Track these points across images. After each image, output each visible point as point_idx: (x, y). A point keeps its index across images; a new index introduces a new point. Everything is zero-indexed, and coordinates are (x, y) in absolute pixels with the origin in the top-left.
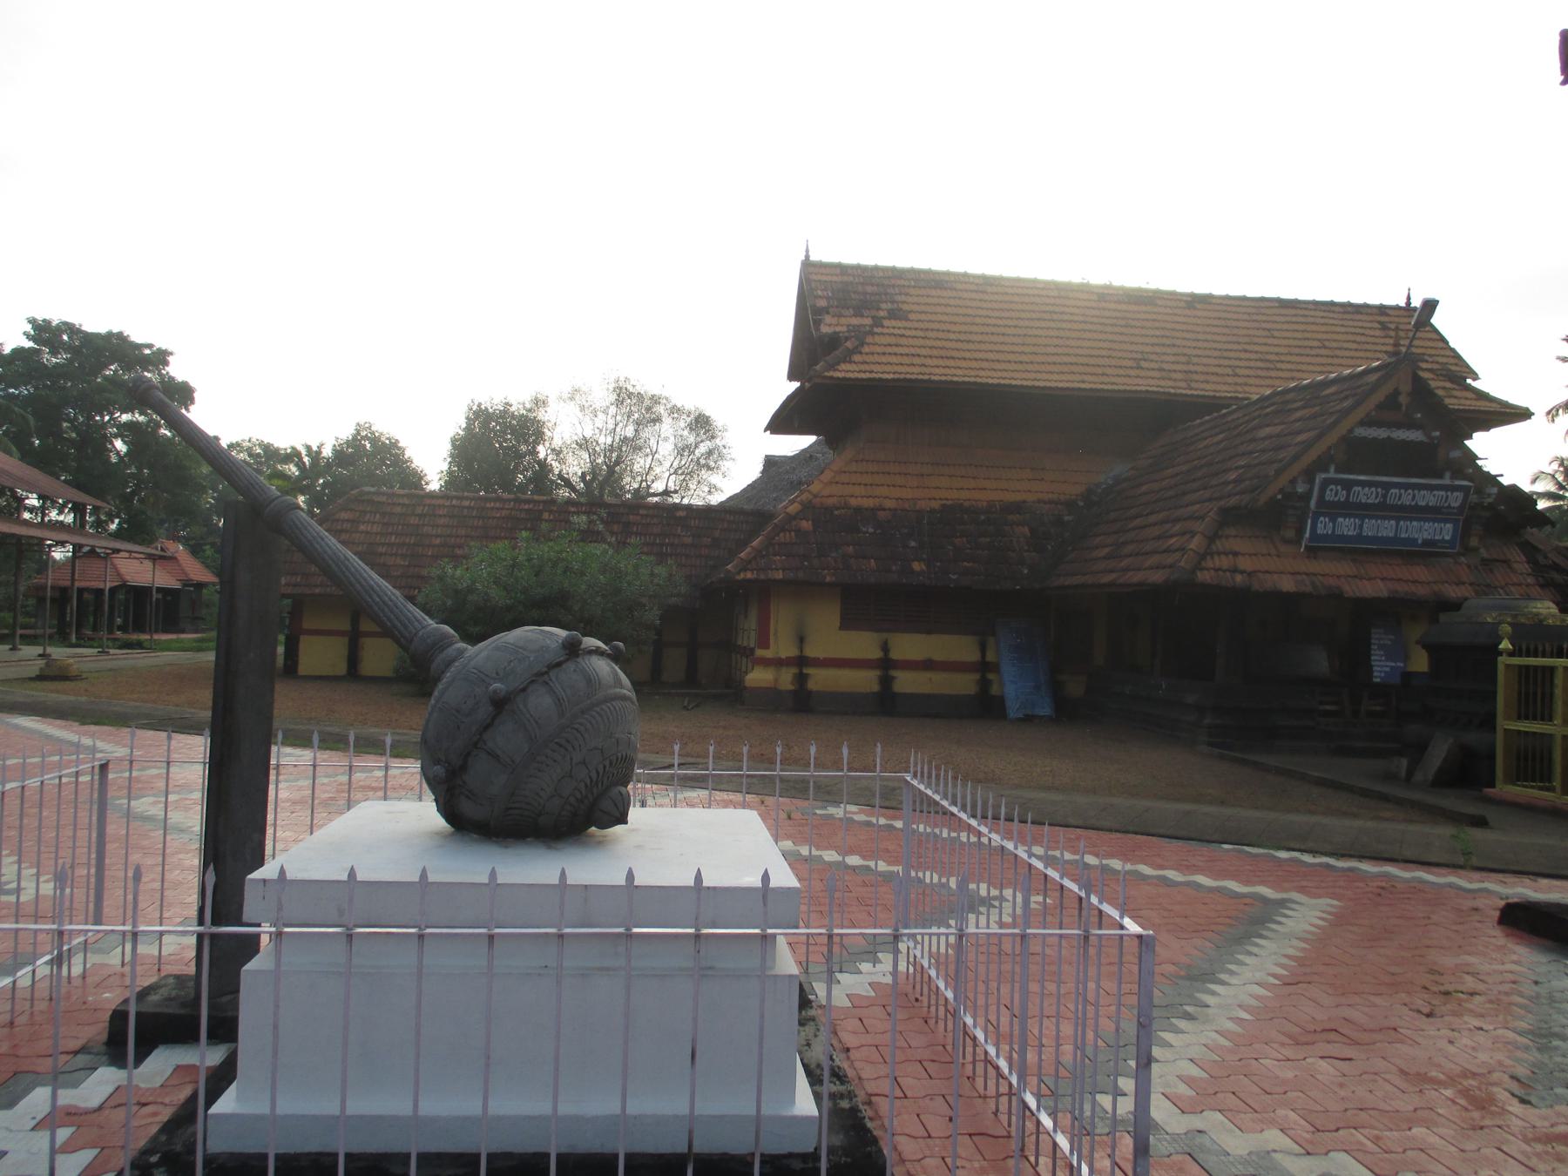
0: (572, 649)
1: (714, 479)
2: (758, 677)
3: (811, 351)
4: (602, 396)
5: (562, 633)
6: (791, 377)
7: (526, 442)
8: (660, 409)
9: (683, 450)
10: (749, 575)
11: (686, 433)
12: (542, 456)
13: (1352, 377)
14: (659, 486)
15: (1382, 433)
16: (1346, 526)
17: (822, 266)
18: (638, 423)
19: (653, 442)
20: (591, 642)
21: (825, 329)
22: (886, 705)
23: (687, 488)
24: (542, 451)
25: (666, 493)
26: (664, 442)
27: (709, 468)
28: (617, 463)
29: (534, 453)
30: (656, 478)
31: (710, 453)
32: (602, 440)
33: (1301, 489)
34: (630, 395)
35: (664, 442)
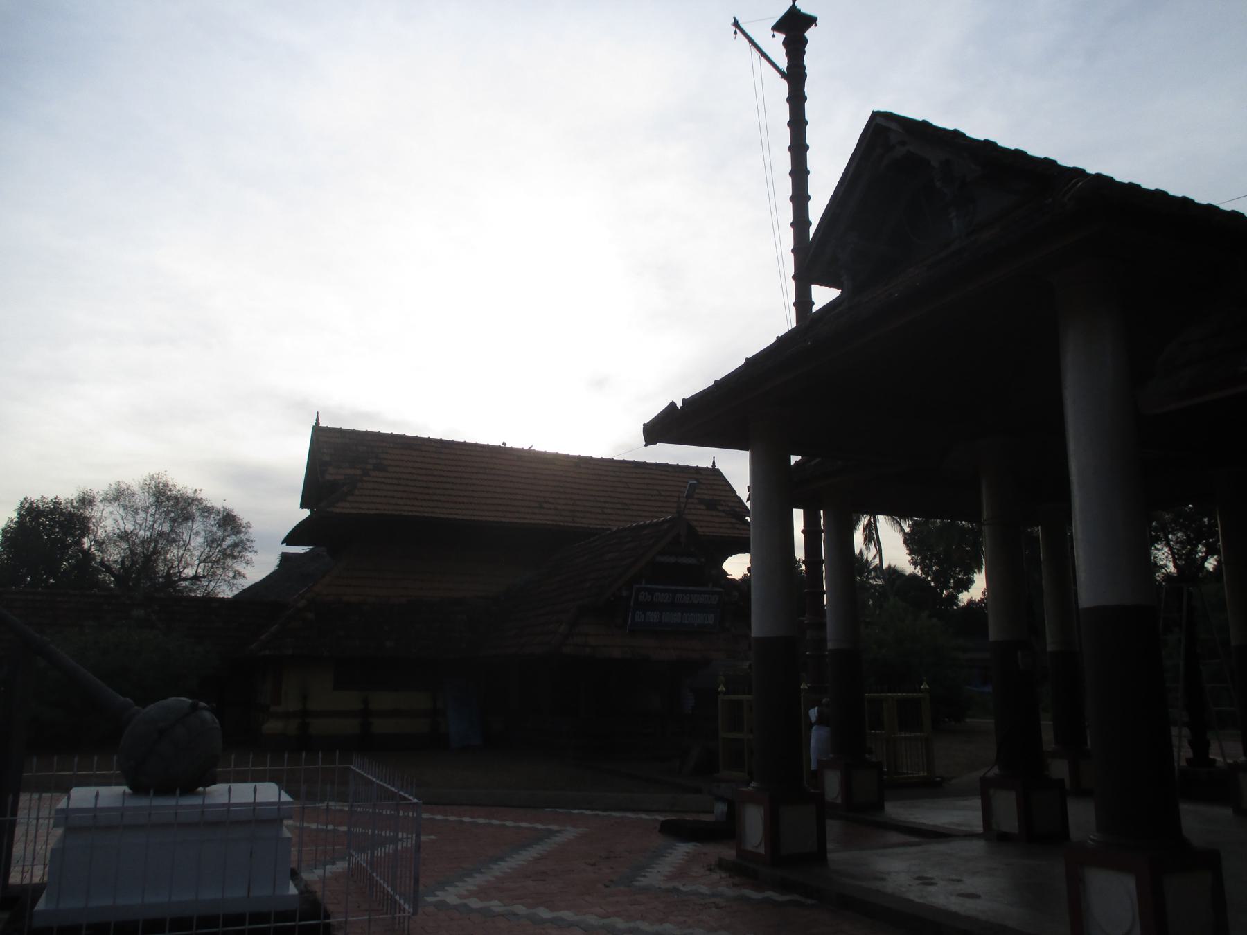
0: (194, 707)
1: (240, 567)
2: (272, 726)
3: (317, 488)
4: (143, 499)
5: (190, 701)
6: (303, 506)
7: (73, 535)
8: (194, 509)
9: (212, 542)
10: (267, 652)
11: (215, 529)
12: (86, 546)
13: (657, 524)
14: (189, 572)
15: (672, 560)
16: (652, 616)
17: (327, 429)
18: (173, 520)
19: (185, 537)
20: (202, 704)
21: (328, 477)
22: (367, 743)
23: (214, 574)
24: (86, 542)
25: (196, 578)
26: (196, 538)
27: (234, 557)
28: (155, 552)
29: (79, 543)
30: (187, 565)
31: (236, 545)
32: (142, 533)
33: (625, 593)
34: (168, 499)
35: (196, 538)
